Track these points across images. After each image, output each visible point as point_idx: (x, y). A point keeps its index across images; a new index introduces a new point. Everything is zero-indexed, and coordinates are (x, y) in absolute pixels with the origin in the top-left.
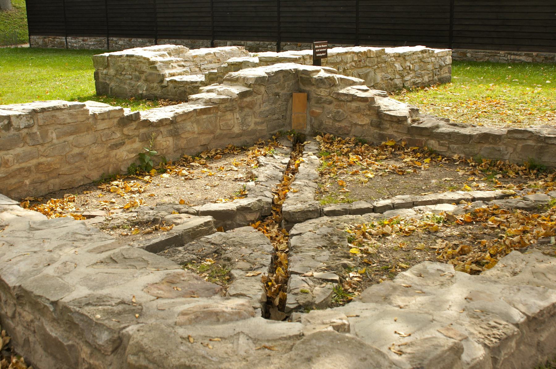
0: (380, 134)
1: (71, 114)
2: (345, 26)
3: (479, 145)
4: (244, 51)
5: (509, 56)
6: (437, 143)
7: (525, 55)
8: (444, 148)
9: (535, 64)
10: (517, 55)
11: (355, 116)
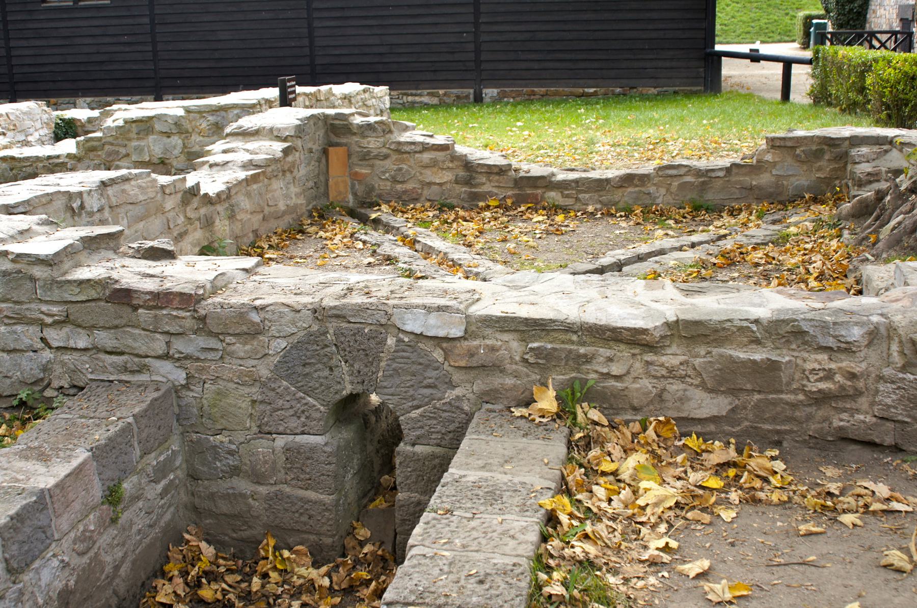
0: (471, 193)
1: (140, 187)
2: (134, 67)
3: (620, 190)
4: (46, 108)
5: (405, 98)
6: (560, 194)
7: (428, 94)
8: (570, 200)
9: (443, 105)
10: (416, 95)
11: (428, 172)
